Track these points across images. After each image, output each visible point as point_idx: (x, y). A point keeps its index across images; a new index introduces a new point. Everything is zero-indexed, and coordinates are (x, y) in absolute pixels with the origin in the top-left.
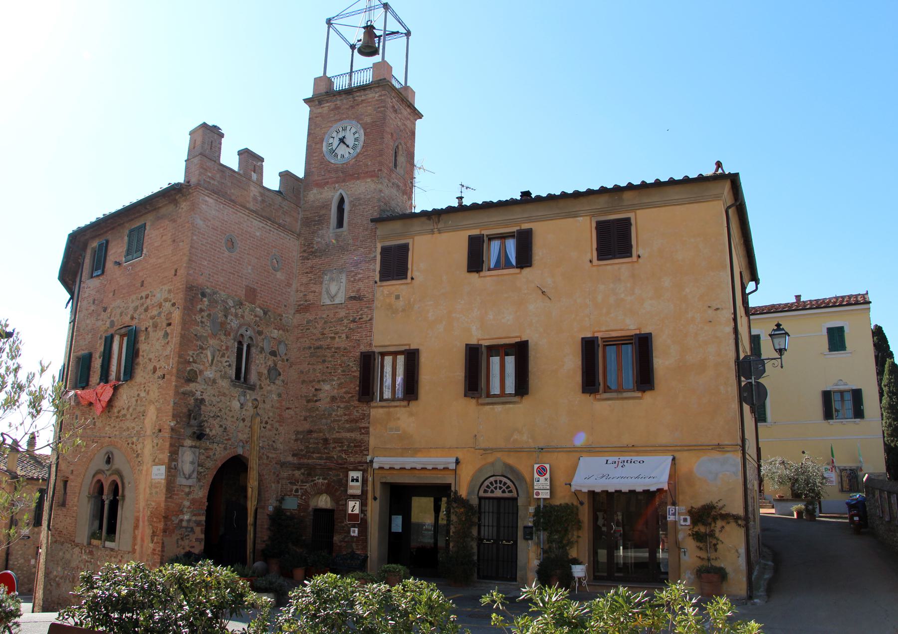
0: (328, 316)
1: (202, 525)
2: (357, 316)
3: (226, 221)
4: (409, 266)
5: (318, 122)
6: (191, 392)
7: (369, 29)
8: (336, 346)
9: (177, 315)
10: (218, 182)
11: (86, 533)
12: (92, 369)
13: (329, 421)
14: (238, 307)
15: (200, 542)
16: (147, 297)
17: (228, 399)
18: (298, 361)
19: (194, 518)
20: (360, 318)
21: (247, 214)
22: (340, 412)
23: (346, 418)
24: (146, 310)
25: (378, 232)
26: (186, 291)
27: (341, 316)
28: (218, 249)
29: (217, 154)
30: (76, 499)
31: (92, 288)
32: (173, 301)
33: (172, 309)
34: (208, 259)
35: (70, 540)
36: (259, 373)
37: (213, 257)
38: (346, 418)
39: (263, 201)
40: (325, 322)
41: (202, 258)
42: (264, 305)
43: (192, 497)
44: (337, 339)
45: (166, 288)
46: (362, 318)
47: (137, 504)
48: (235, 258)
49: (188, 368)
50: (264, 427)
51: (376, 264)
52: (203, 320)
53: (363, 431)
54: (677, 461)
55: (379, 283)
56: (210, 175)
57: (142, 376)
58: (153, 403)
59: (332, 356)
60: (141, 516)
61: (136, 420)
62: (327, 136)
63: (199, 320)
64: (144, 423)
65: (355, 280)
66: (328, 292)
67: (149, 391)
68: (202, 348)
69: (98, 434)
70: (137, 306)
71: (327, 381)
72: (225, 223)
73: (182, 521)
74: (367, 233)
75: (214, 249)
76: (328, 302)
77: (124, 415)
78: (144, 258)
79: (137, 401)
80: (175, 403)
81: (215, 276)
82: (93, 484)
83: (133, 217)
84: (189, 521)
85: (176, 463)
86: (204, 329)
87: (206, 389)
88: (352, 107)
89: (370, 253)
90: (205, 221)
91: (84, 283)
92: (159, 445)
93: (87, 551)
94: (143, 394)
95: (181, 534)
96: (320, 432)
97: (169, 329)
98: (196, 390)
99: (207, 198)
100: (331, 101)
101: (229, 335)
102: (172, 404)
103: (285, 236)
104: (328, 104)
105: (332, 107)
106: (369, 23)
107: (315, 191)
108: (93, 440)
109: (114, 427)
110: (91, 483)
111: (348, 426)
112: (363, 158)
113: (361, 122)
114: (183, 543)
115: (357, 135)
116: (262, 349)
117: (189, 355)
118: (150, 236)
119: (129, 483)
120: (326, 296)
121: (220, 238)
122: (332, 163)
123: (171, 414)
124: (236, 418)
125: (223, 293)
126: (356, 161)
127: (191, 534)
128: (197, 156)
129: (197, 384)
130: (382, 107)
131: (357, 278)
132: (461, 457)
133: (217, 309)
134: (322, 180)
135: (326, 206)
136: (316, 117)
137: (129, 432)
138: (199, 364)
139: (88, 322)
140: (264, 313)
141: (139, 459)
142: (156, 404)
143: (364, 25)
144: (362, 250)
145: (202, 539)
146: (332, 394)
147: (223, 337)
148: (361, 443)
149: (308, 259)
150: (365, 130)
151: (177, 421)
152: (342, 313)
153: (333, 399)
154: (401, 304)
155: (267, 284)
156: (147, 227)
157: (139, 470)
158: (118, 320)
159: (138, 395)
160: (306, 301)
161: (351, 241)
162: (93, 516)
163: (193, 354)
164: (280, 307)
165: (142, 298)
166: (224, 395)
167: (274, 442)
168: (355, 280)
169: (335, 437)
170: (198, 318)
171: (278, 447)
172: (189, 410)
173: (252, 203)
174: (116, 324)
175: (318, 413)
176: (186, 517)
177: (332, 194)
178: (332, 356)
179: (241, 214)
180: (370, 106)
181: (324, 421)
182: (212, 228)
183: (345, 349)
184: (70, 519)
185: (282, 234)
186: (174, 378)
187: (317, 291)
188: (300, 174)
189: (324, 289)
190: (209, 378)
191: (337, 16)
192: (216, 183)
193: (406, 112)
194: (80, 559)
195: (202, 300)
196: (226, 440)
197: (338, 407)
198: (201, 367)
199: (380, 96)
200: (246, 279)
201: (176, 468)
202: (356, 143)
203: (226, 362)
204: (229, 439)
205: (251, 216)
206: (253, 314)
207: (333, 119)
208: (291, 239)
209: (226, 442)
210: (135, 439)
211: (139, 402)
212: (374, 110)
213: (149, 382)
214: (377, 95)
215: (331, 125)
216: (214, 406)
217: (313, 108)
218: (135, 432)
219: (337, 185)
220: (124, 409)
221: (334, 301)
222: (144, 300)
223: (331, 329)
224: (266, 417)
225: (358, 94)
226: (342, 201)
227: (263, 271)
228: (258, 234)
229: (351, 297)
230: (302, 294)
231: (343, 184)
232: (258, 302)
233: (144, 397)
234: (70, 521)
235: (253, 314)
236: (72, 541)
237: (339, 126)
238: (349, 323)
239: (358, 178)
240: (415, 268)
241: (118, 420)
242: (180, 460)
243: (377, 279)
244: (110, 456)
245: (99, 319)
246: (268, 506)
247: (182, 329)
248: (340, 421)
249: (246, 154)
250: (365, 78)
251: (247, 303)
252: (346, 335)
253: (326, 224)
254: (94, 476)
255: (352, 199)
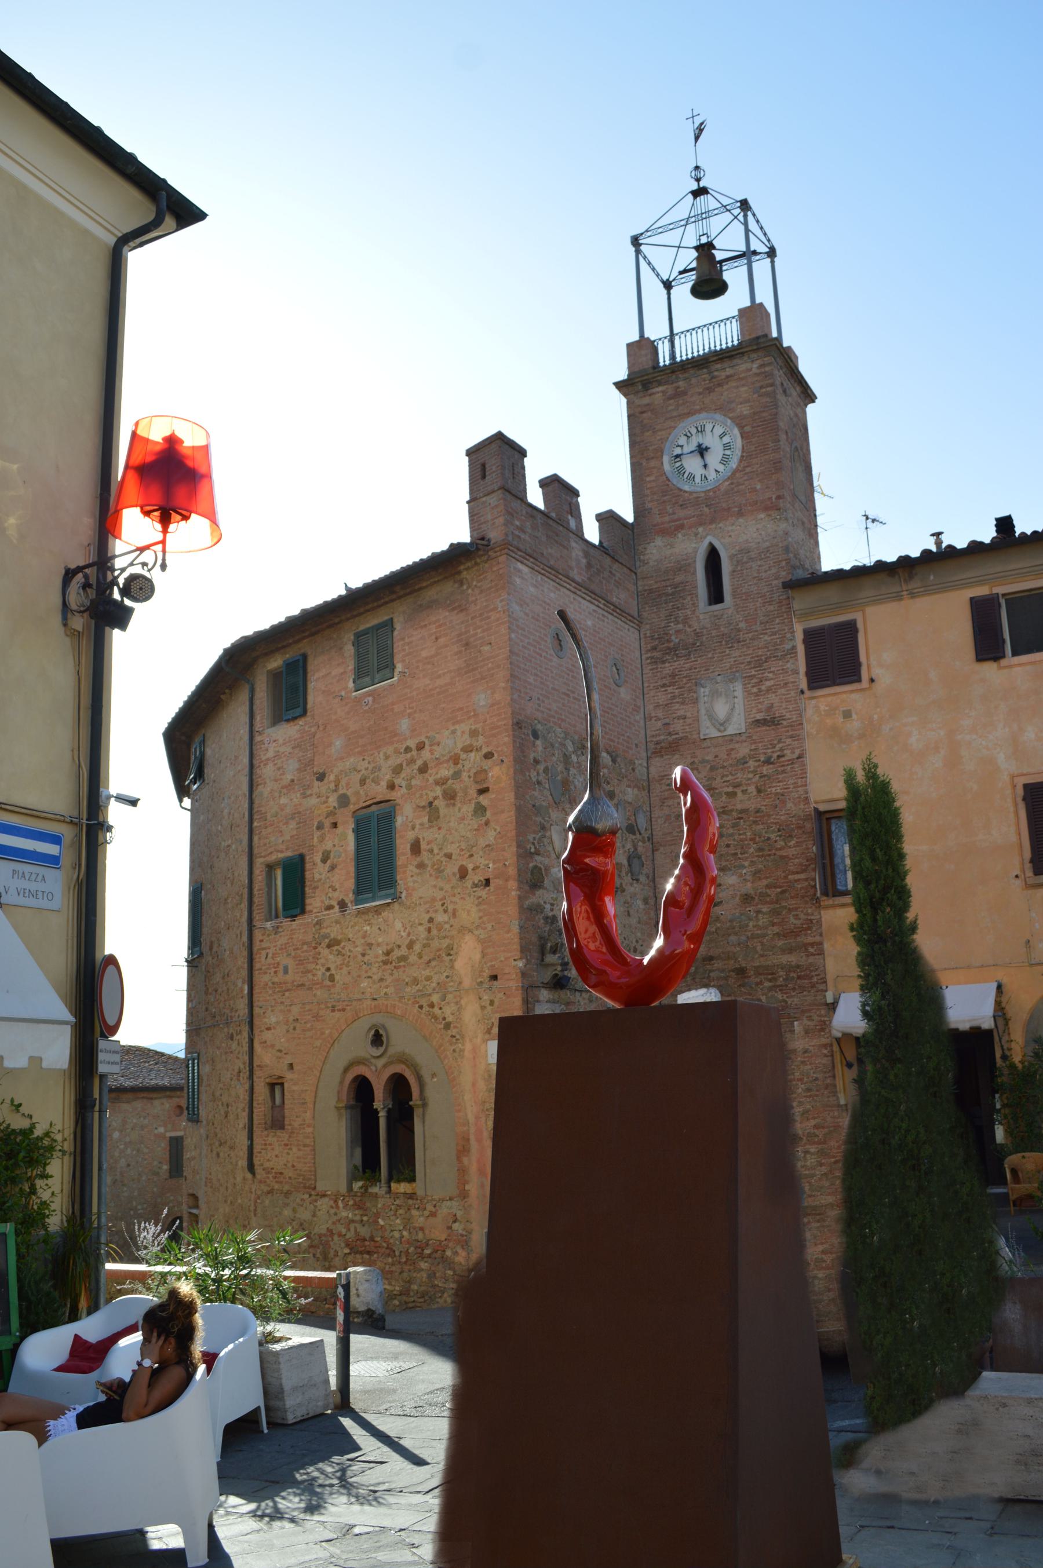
0: (716, 756)
2: (773, 752)
3: (548, 604)
4: (863, 658)
5: (645, 421)
7: (705, 250)
8: (739, 807)
9: (500, 775)
11: (344, 1171)
12: (308, 883)
13: (743, 938)
14: (579, 753)
16: (421, 747)
18: (669, 838)
20: (779, 757)
22: (763, 920)
23: (776, 929)
24: (423, 769)
25: (796, 605)
26: (514, 730)
27: (740, 755)
28: (544, 654)
30: (308, 1115)
31: (281, 741)
32: (485, 750)
33: (487, 764)
35: (305, 1187)
37: (539, 668)
38: (776, 929)
40: (713, 768)
42: (610, 746)
44: (740, 794)
45: (465, 727)
46: (783, 756)
47: (459, 1111)
48: (567, 668)
49: (531, 865)
51: (797, 660)
53: (811, 950)
54: (1004, 989)
55: (808, 693)
56: (517, 523)
57: (435, 886)
58: (470, 931)
59: (734, 826)
60: (472, 1130)
61: (433, 963)
62: (668, 444)
64: (452, 967)
65: (760, 691)
66: (711, 717)
67: (455, 911)
69: (343, 996)
70: (401, 765)
71: (730, 870)
72: (547, 607)
74: (771, 608)
75: (538, 654)
76: (715, 733)
77: (403, 958)
78: (399, 680)
79: (429, 930)
80: (521, 927)
81: (546, 701)
82: (345, 1089)
83: (375, 604)
88: (710, 390)
89: (782, 643)
90: (521, 605)
91: (260, 733)
92: (496, 1003)
93: (351, 1203)
94: (441, 918)
96: (729, 958)
97: (484, 800)
98: (545, 902)
99: (520, 566)
100: (666, 383)
102: (516, 929)
103: (623, 624)
104: (661, 388)
105: (670, 392)
106: (704, 240)
107: (659, 541)
108: (333, 1007)
109: (381, 980)
110: (341, 1082)
111: (780, 943)
112: (746, 478)
113: (731, 415)
115: (726, 439)
118: (407, 640)
119: (434, 1075)
120: (708, 724)
122: (685, 492)
123: (517, 947)
126: (732, 484)
128: (493, 492)
129: (545, 891)
130: (768, 386)
131: (763, 688)
132: (1005, 981)
134: (669, 522)
135: (684, 566)
136: (642, 413)
137: (419, 987)
139: (283, 800)
141: (453, 1031)
142: (476, 932)
143: (695, 244)
144: (766, 638)
146: (743, 891)
148: (811, 971)
149: (663, 662)
150: (741, 427)
151: (527, 960)
152: (744, 750)
153: (747, 899)
154: (854, 725)
156: (398, 626)
157: (454, 1051)
158: (357, 793)
159: (431, 920)
160: (670, 734)
161: (742, 625)
162: (352, 1142)
164: (631, 749)
165: (408, 750)
168: (760, 691)
169: (758, 964)
172: (541, 938)
173: (576, 571)
174: (353, 799)
175: (719, 925)
177: (694, 545)
178: (734, 826)
179: (565, 590)
180: (743, 385)
181: (733, 939)
182: (533, 617)
183: (758, 811)
184: (299, 1150)
185: (619, 622)
186: (513, 884)
187: (689, 714)
188: (629, 517)
189: (703, 712)
191: (647, 231)
193: (795, 392)
194: (335, 1218)
197: (758, 912)
198: (546, 861)
199: (762, 366)
202: (728, 452)
207: (675, 414)
210: (435, 998)
211: (434, 932)
212: (754, 393)
213: (454, 895)
214: (755, 366)
215: (673, 424)
217: (632, 396)
218: (434, 985)
219: (700, 529)
220: (399, 946)
221: (725, 730)
222: (414, 753)
223: (725, 779)
224: (634, 941)
225: (719, 366)
226: (713, 558)
228: (589, 623)
229: (758, 721)
230: (659, 724)
231: (714, 526)
233: (446, 923)
234: (301, 1154)
236: (309, 1188)
237: (689, 425)
238: (759, 766)
239: (740, 514)
240: (873, 662)
241: (388, 966)
243: (803, 684)
244: (381, 1032)
245: (311, 795)
247: (516, 798)
248: (764, 936)
249: (556, 484)
250: (729, 336)
252: (757, 787)
253: (689, 598)
254: (346, 1070)
255: (733, 551)
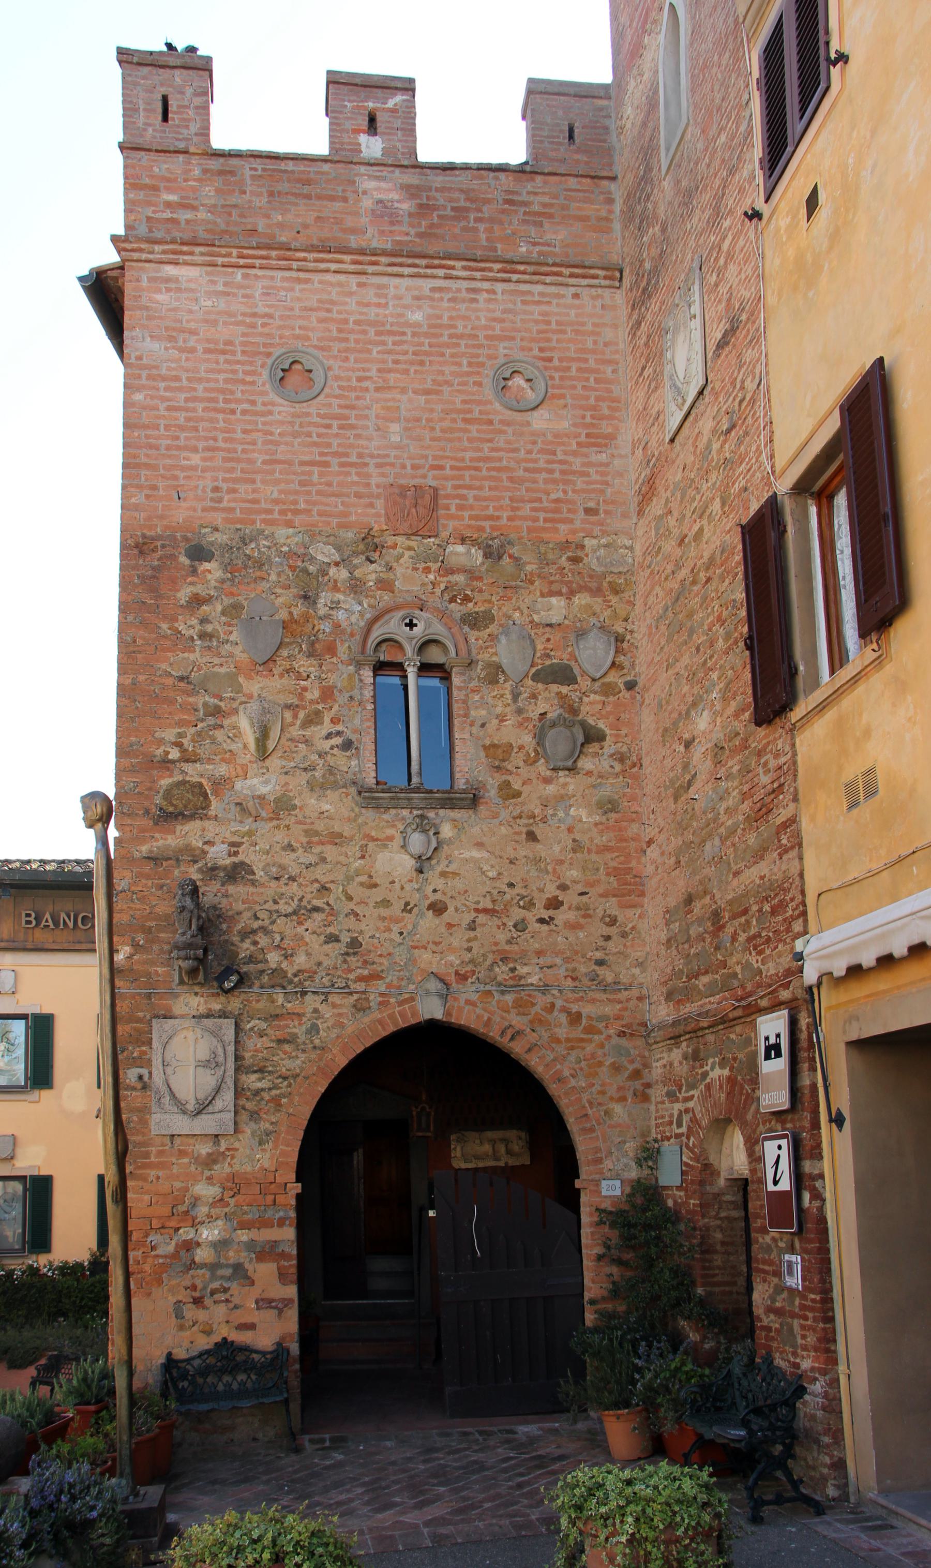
1: (284, 1255)
6: (188, 849)
10: (212, 209)
15: (280, 1312)
17: (353, 850)
19: (244, 1236)
21: (352, 268)
29: (194, 128)
34: (201, 445)
36: (490, 749)
39: (424, 209)
41: (179, 448)
43: (228, 1170)
49: (165, 782)
50: (542, 921)
52: (209, 628)
63: (193, 633)
68: (216, 712)
73: (189, 1246)
75: (223, 411)
84: (221, 1245)
85: (144, 1072)
86: (219, 655)
87: (250, 833)
90: (171, 339)
95: (194, 1288)
99: (170, 270)
101: (331, 650)
114: (201, 1315)
116: (495, 673)
117: (161, 741)
121: (246, 373)
124: (398, 906)
125: (282, 533)
127: (234, 1286)
133: (265, 585)
138: (210, 761)
140: (487, 556)
145: (287, 1302)
147: (304, 664)
155: (487, 459)
163: (180, 735)
166: (336, 839)
167: (600, 963)
170: (188, 626)
171: (624, 979)
176: (208, 1234)
179: (329, 277)
185: (539, 288)
190: (262, 798)
192: (202, 215)
195: (194, 571)
196: (360, 979)
198: (223, 770)
200: (378, 466)
201: (145, 1087)
203: (329, 736)
204: (376, 976)
205: (370, 269)
206: (434, 566)
208: (585, 292)
209: (361, 986)
216: (292, 879)
227: (461, 425)
228: (416, 316)
232: (449, 527)
235: (434, 566)
242: (157, 1061)
246: (597, 1183)
251: (400, 540)
